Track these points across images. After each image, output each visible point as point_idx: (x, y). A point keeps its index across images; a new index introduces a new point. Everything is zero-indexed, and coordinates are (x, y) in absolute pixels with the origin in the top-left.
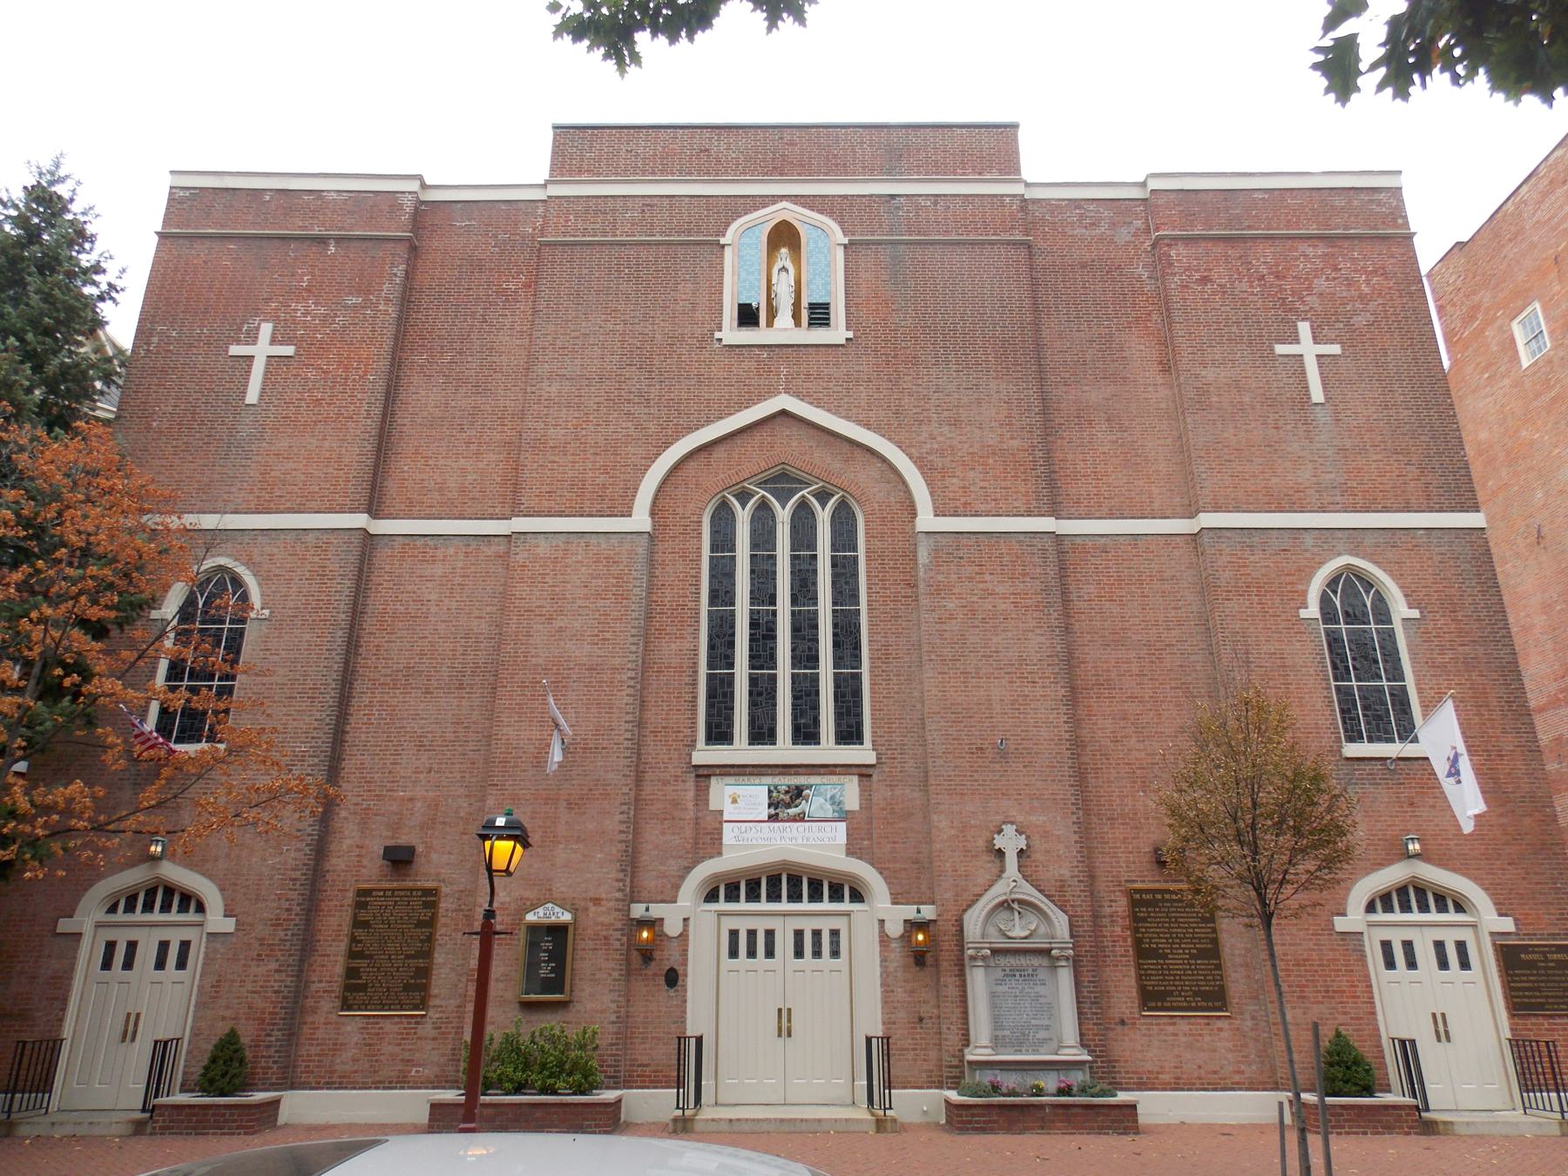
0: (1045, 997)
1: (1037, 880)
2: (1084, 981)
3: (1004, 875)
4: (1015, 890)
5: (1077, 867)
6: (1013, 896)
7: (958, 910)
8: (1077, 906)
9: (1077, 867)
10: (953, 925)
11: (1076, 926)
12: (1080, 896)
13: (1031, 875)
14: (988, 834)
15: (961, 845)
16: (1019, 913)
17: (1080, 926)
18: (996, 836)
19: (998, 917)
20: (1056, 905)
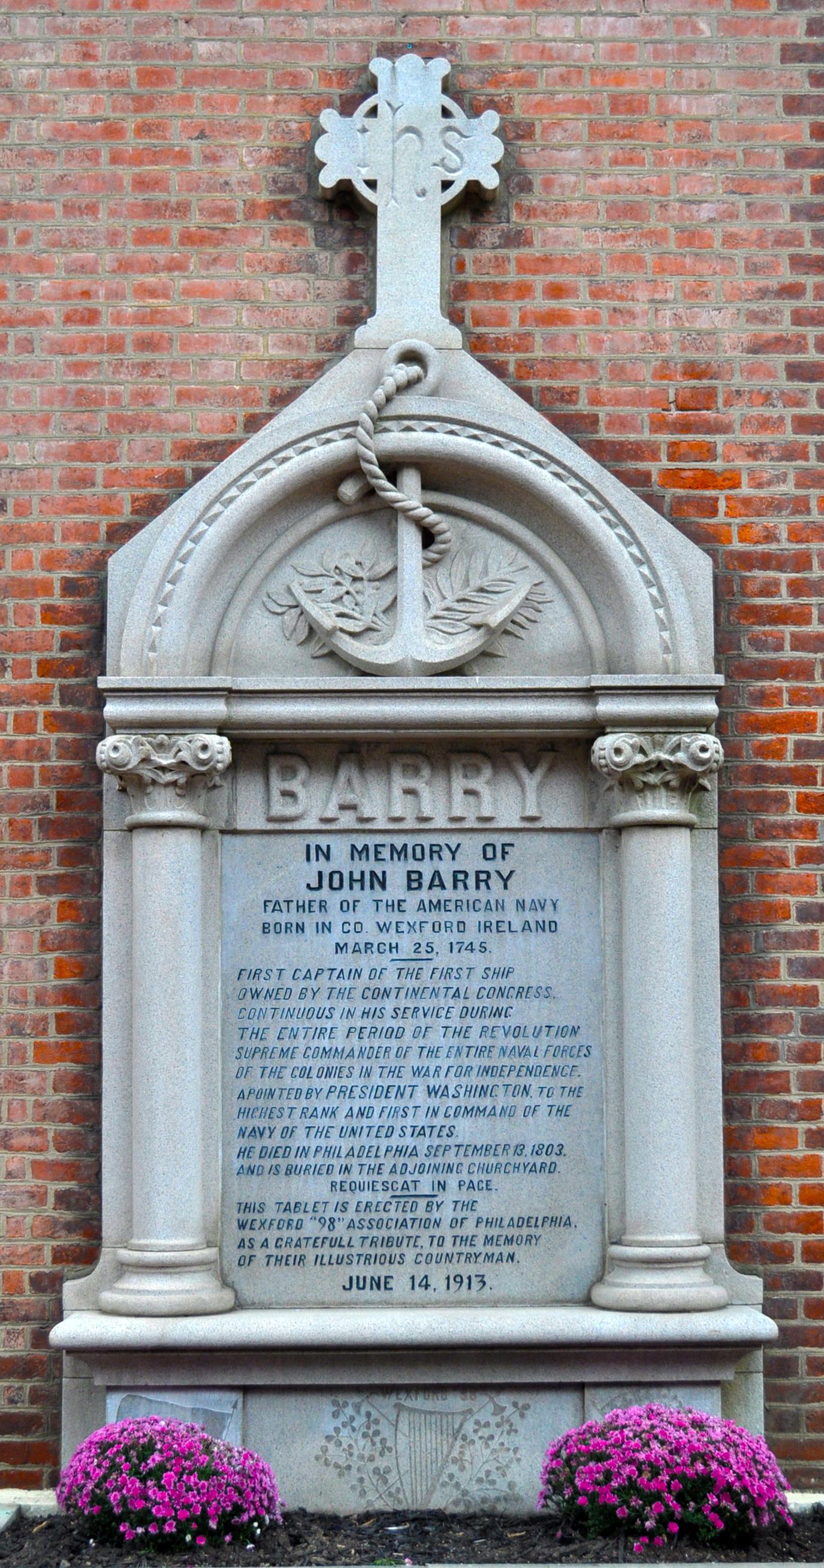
0: (546, 993)
1: (554, 368)
2: (782, 912)
3: (363, 334)
4: (409, 404)
5: (792, 291)
6: (395, 440)
7: (87, 533)
8: (775, 505)
9: (792, 291)
10: (50, 614)
11: (757, 615)
12: (791, 453)
13: (523, 342)
14: (294, 121)
15: (126, 173)
16: (428, 537)
17: (783, 616)
18: (329, 118)
19: (309, 559)
20: (654, 501)
